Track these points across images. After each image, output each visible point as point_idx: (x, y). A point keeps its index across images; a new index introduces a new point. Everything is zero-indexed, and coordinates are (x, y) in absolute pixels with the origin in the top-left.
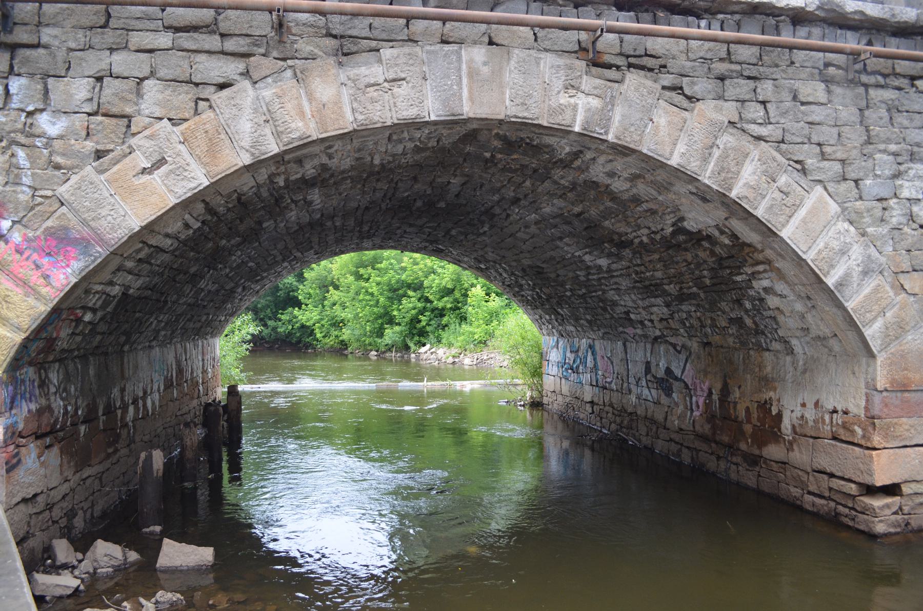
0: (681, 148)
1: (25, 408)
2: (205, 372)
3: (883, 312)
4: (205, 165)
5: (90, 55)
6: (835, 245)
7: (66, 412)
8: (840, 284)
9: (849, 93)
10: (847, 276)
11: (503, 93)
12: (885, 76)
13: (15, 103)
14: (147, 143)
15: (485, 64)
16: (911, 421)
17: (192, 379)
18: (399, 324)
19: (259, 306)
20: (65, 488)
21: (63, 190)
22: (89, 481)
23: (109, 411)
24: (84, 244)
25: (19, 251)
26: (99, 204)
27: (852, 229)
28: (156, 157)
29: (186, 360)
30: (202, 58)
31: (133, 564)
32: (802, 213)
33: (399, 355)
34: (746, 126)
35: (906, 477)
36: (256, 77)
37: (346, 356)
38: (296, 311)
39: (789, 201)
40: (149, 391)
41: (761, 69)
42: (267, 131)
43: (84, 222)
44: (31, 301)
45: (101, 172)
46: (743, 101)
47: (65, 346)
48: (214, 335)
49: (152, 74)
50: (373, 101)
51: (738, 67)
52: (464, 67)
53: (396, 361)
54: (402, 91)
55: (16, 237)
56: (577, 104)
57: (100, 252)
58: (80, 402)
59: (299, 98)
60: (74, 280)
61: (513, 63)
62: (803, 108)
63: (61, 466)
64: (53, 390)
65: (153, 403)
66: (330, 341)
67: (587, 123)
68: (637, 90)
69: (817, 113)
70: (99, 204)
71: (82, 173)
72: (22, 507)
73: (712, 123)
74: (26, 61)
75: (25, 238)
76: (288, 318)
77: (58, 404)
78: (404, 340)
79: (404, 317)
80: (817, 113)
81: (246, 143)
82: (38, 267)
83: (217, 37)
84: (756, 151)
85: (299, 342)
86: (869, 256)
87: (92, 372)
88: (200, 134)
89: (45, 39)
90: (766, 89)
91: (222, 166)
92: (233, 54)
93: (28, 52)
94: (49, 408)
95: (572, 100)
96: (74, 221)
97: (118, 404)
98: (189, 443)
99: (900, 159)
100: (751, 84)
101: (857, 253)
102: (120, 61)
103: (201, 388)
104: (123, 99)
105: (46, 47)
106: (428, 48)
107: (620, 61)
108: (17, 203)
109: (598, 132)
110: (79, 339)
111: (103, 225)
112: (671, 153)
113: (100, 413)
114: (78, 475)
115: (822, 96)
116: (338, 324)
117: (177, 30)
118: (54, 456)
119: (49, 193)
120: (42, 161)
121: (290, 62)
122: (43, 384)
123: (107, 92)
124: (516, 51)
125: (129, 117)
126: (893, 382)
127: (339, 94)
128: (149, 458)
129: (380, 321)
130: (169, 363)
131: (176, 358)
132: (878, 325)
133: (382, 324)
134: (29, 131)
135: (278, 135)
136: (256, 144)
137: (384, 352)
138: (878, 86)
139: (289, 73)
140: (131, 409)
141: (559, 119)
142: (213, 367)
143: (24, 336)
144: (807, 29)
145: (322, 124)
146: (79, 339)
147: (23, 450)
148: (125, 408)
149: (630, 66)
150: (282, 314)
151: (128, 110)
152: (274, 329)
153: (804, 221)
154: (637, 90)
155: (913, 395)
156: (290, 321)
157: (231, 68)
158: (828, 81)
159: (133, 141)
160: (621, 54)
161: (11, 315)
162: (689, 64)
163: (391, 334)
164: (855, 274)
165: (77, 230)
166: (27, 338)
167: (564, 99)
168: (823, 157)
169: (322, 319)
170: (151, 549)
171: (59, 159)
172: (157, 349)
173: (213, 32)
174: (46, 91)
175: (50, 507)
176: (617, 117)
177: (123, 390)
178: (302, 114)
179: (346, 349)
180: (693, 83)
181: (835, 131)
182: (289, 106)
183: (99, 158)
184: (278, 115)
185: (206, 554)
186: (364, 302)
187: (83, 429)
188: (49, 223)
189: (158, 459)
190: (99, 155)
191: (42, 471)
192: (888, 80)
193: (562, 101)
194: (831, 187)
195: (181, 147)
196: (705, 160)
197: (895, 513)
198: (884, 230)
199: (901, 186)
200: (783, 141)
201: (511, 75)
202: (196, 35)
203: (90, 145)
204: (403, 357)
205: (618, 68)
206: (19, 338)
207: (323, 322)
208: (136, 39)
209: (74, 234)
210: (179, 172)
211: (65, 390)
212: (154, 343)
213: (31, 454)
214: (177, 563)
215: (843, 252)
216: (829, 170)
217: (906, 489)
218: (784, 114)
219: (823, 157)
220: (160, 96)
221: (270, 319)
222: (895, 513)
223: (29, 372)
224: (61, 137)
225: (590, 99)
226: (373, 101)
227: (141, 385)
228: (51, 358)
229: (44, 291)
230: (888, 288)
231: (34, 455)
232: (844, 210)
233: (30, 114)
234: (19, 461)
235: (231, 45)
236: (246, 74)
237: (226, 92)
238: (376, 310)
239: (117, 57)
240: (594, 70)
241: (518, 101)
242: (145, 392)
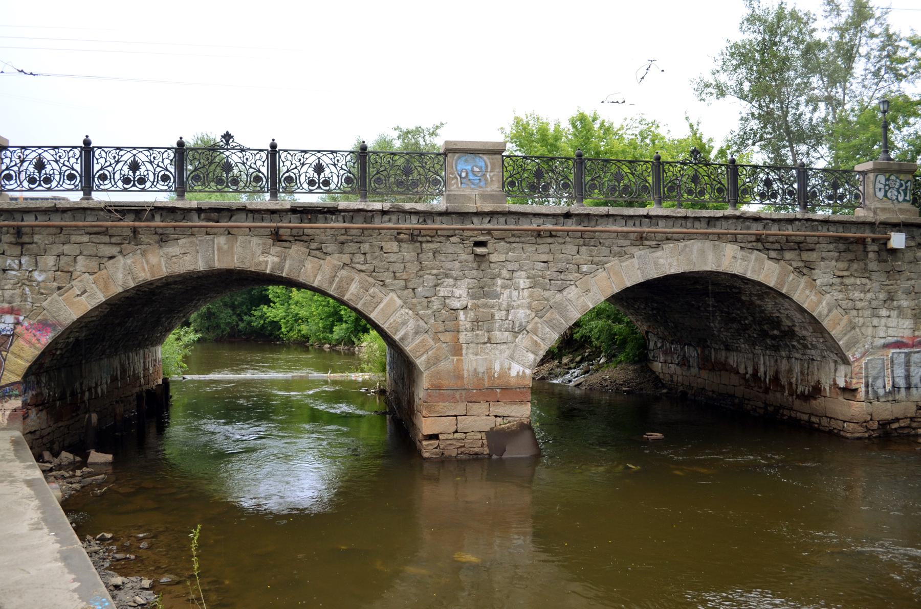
0: (319, 278)
1: (31, 393)
2: (146, 369)
3: (427, 351)
4: (103, 292)
5: (54, 246)
6: (399, 320)
7: (49, 395)
8: (402, 339)
9: (411, 246)
10: (406, 335)
11: (233, 257)
12: (432, 237)
13: (24, 268)
14: (79, 284)
15: (225, 244)
16: (444, 404)
17: (134, 374)
18: (346, 322)
19: (236, 303)
20: (49, 430)
21: (45, 304)
22: (61, 429)
23: (73, 394)
24: (53, 326)
25: (27, 329)
26: (59, 310)
27: (411, 312)
28: (83, 290)
30: (101, 246)
31: (78, 462)
32: (382, 305)
33: (346, 347)
34: (354, 265)
35: (439, 432)
36: (125, 253)
37: (308, 347)
38: (265, 308)
39: (375, 300)
40: (99, 384)
41: (363, 238)
42: (129, 277)
43: (54, 317)
44: (32, 350)
45: (60, 296)
46: (353, 254)
47: (48, 365)
48: (156, 345)
49: (81, 253)
50: (175, 263)
51: (351, 238)
52: (216, 246)
53: (344, 352)
54: (187, 258)
55: (26, 324)
57: (60, 329)
58: (56, 390)
59: (142, 263)
60: (50, 341)
61: (238, 243)
62: (385, 255)
63: (47, 419)
64: (43, 385)
65: (102, 390)
66: (294, 335)
67: (272, 269)
68: (296, 253)
69: (393, 257)
70: (59, 310)
71: (53, 296)
72: (29, 435)
73: (334, 266)
74: (28, 250)
75: (30, 324)
76: (260, 314)
77: (46, 391)
78: (349, 337)
79: (350, 316)
80: (393, 257)
81: (120, 283)
82: (35, 336)
83: (108, 237)
84: (357, 277)
85: (271, 334)
86: (418, 325)
87: (63, 375)
88: (101, 280)
89: (35, 240)
90: (366, 247)
91: (111, 293)
92: (115, 244)
93: (29, 246)
94: (41, 394)
95: (266, 259)
96: (49, 317)
97: (79, 391)
98: (118, 412)
99: (439, 277)
100: (358, 245)
101: (411, 324)
102: (67, 248)
103: (142, 380)
104: (68, 265)
105: (36, 243)
106: (199, 238)
107: (291, 239)
108: (26, 309)
109: (278, 273)
110: (55, 362)
111: (61, 318)
112: (314, 281)
113: (68, 395)
114: (56, 425)
115: (396, 249)
116: (297, 319)
117: (90, 234)
118: (43, 414)
119: (39, 305)
120: (36, 291)
121: (139, 247)
122: (39, 383)
123: (62, 262)
124: (240, 237)
125: (71, 272)
126: (433, 385)
127: (160, 260)
128: (90, 417)
129: (331, 319)
130: (115, 366)
131: (120, 362)
132: (424, 357)
133: (333, 322)
134: (30, 279)
135: (134, 279)
136: (124, 283)
137: (336, 345)
138: (428, 242)
139: (139, 251)
140: (87, 394)
141: (259, 268)
142: (155, 365)
143: (30, 364)
144: (388, 217)
145: (152, 274)
146: (55, 362)
147: (30, 411)
148: (83, 393)
149: (296, 240)
150: (255, 310)
151: (71, 269)
152: (249, 323)
153: (382, 309)
154: (296, 253)
155: (446, 391)
156: (261, 317)
157: (114, 250)
158: (399, 241)
159: (74, 283)
160: (291, 235)
161: (24, 355)
162: (325, 238)
163: (339, 331)
165: (51, 320)
166: (31, 365)
167: (261, 259)
168: (395, 278)
169: (288, 316)
170: (86, 456)
171: (43, 291)
172: (106, 360)
173: (106, 235)
174: (36, 262)
175: (42, 437)
177: (81, 384)
178: (144, 270)
179: (308, 341)
180: (326, 246)
181: (402, 265)
182: (138, 267)
184: (133, 271)
185: (109, 457)
186: (318, 303)
187: (58, 403)
188: (39, 318)
189: (94, 417)
190: (59, 288)
191: (38, 421)
192: (433, 239)
193: (261, 260)
194: (399, 292)
195: (93, 285)
196: (331, 283)
197: (436, 448)
198: (429, 312)
199: (439, 290)
200: (374, 271)
201: (238, 249)
202: (99, 236)
203: (55, 284)
204: (349, 350)
205: (290, 241)
206: (28, 365)
207: (288, 319)
208: (74, 238)
209: (50, 322)
210: (92, 296)
211: (49, 385)
212: (103, 356)
213: (33, 414)
214: (96, 461)
215: (404, 323)
216: (397, 284)
217: (441, 437)
218: (375, 259)
219: (395, 278)
220: (84, 263)
221: (246, 314)
222: (436, 448)
223: (32, 378)
224: (43, 281)
225: (274, 258)
226: (175, 263)
227: (94, 380)
228: (42, 371)
229: (38, 345)
230: (430, 340)
231: (34, 413)
232: (405, 303)
233: (30, 272)
234: (28, 416)
235: (114, 240)
236: (121, 252)
237: (111, 261)
238: (326, 309)
240: (278, 243)
241: (240, 260)
242: (97, 384)
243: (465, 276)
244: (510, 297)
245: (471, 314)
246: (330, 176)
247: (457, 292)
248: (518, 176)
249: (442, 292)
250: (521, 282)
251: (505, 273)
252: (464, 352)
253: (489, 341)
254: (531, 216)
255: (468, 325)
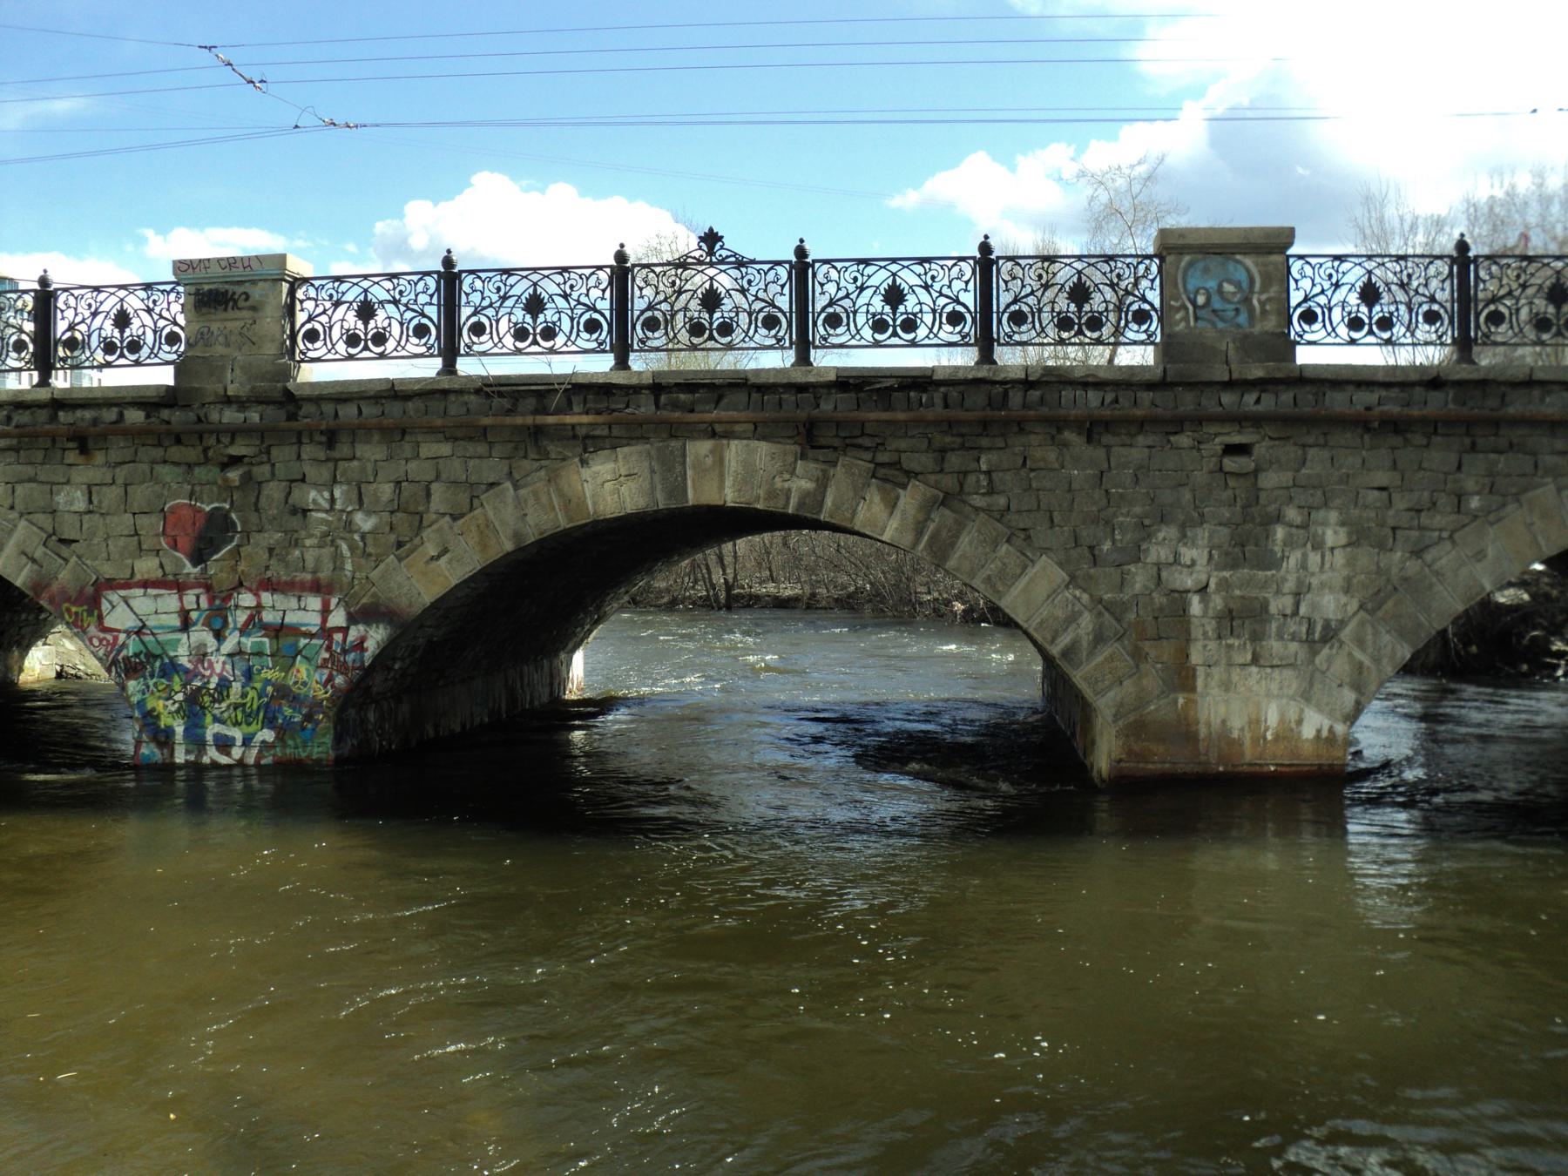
29: (522, 687)
56: (789, 490)
151: (421, 509)
164: (1085, 644)
176: (829, 501)
183: (398, 549)
215: (1072, 618)
239: (413, 465)
243: (1202, 519)
244: (1303, 565)
245: (1217, 602)
246: (555, 318)
247: (1187, 554)
248: (847, 303)
249: (1157, 552)
250: (1329, 533)
251: (1292, 514)
252: (1200, 682)
253: (1255, 660)
254: (1351, 388)
255: (1210, 627)
